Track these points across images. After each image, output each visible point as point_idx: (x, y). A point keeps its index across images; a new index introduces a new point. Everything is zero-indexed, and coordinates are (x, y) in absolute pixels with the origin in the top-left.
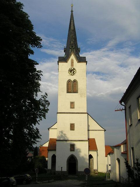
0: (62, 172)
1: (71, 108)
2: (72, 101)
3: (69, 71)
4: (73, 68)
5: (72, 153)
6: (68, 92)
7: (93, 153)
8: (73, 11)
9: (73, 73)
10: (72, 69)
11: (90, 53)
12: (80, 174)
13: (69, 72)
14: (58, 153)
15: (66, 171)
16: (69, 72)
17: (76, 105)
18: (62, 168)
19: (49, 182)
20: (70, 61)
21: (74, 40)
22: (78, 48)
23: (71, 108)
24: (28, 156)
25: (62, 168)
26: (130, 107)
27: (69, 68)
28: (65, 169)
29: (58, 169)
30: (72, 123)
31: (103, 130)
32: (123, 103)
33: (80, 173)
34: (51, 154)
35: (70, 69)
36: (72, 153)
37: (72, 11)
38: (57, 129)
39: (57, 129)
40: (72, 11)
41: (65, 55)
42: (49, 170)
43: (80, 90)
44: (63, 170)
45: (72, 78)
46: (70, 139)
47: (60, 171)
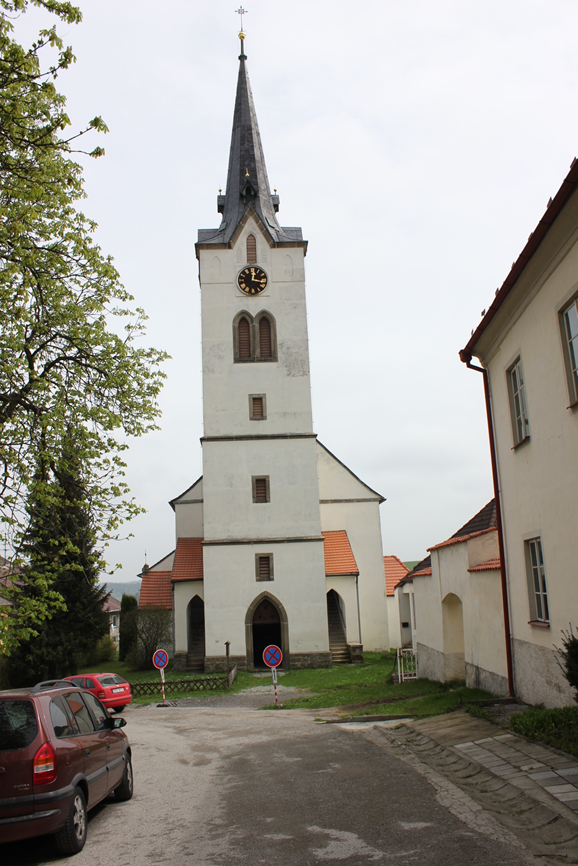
3: (240, 277)
5: (266, 587)
6: (237, 361)
7: (344, 589)
8: (246, 58)
9: (250, 273)
11: (277, 737)
14: (212, 594)
15: (244, 653)
17: (270, 407)
18: (227, 644)
20: (241, 242)
25: (227, 644)
26: (511, 373)
28: (240, 648)
29: (213, 648)
30: (261, 473)
31: (374, 500)
32: (475, 361)
33: (299, 660)
34: (182, 599)
36: (266, 587)
43: (284, 349)
44: (233, 652)
45: (254, 306)
46: (442, 563)
47: (222, 659)
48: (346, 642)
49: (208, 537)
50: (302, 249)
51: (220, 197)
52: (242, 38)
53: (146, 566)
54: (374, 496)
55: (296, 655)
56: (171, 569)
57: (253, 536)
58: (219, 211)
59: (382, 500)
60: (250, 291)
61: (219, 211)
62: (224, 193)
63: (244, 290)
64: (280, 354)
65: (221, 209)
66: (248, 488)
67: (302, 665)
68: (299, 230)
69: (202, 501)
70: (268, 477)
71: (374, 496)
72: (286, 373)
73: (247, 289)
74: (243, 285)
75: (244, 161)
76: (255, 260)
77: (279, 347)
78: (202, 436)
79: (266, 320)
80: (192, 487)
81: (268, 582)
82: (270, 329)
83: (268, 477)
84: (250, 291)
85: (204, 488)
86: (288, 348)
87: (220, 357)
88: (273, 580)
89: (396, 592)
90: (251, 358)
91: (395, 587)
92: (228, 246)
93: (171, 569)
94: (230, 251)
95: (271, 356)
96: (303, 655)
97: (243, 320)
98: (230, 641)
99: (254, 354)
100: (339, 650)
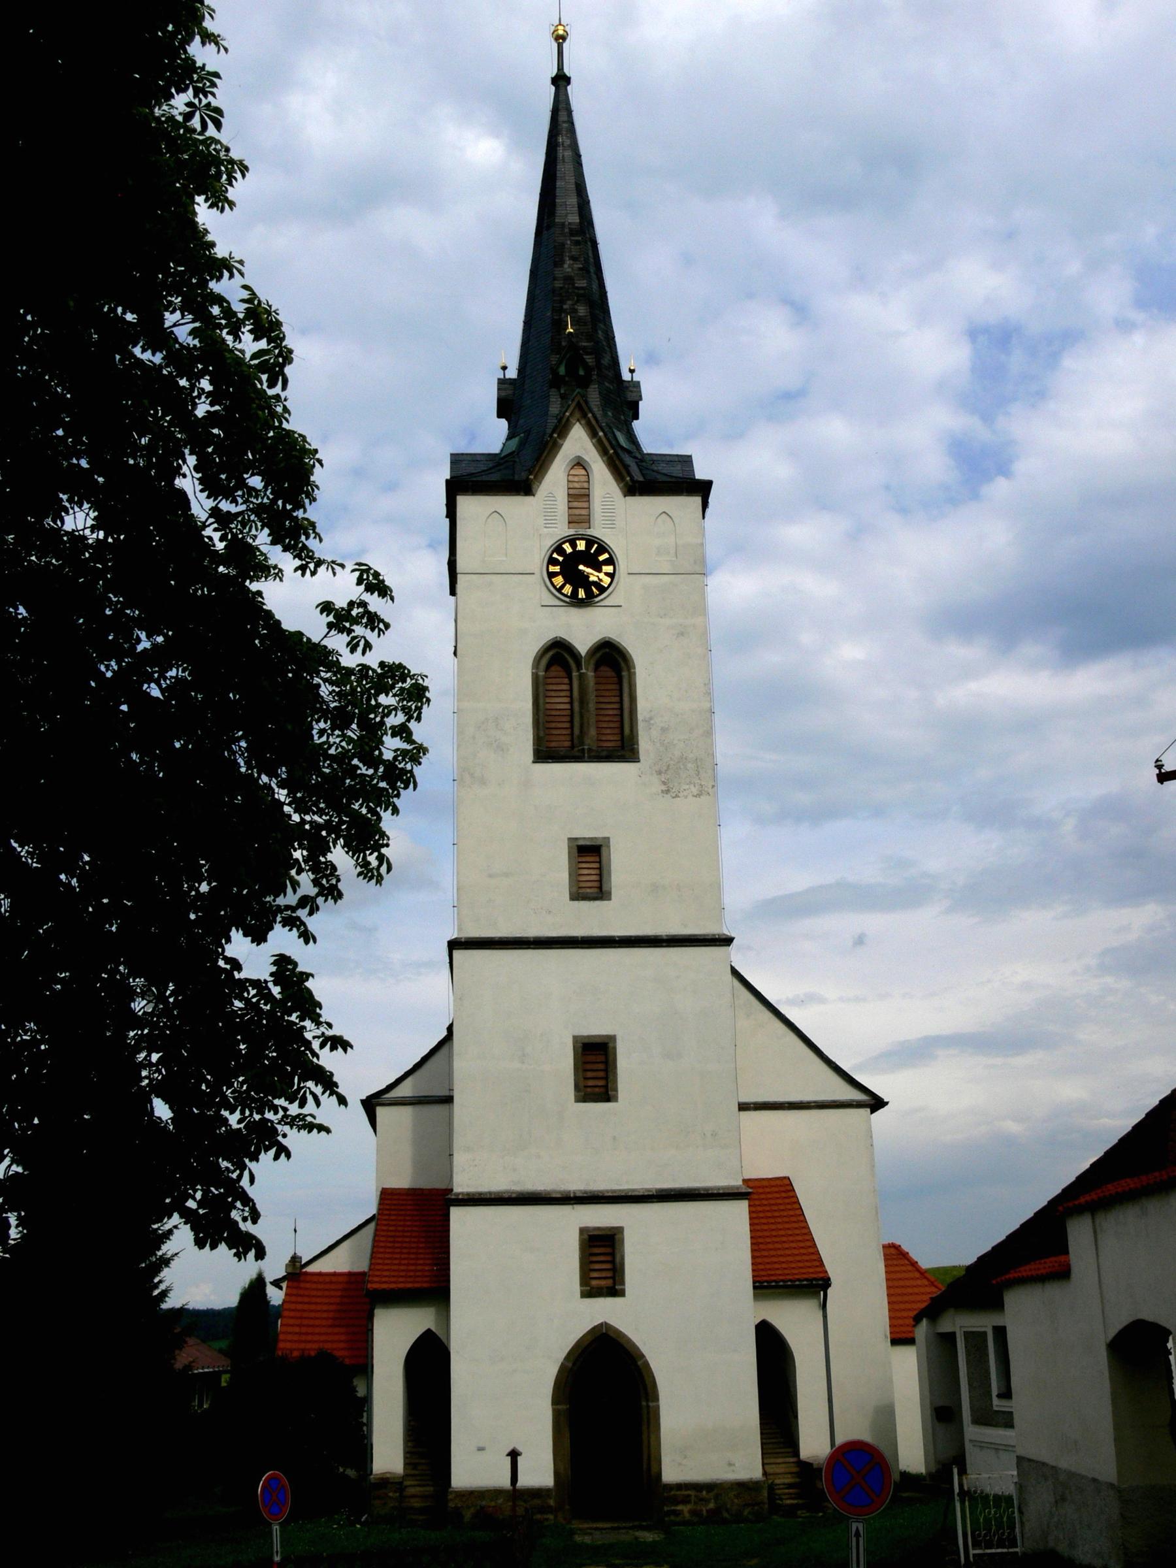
0: (516, 1494)
1: (578, 894)
2: (587, 832)
3: (552, 561)
4: (590, 542)
6: (545, 753)
8: (567, 80)
10: (581, 545)
12: (685, 1509)
13: (551, 575)
16: (551, 575)
18: (514, 1455)
19: (303, 1350)
21: (582, 310)
22: (626, 376)
23: (578, 894)
24: (247, 360)
25: (514, 1455)
27: (549, 542)
30: (596, 1029)
31: (858, 1105)
33: (686, 1500)
35: (559, 549)
36: (604, 1311)
37: (561, 80)
38: (743, 1107)
39: (743, 1107)
40: (561, 80)
41: (509, 438)
42: (385, 1482)
43: (655, 733)
44: (527, 1480)
47: (497, 1493)
48: (796, 1453)
49: (462, 1184)
50: (698, 500)
51: (502, 382)
52: (560, 39)
53: (295, 1259)
54: (851, 1094)
55: (680, 1486)
56: (366, 1269)
57: (575, 1184)
58: (499, 416)
59: (876, 1103)
60: (575, 593)
61: (499, 416)
62: (512, 373)
63: (560, 590)
64: (645, 744)
65: (505, 408)
66: (565, 1063)
67: (693, 1513)
68: (687, 461)
69: (448, 1100)
70: (613, 1038)
71: (851, 1094)
72: (657, 787)
73: (568, 589)
74: (559, 581)
75: (562, 302)
76: (587, 521)
77: (641, 726)
78: (454, 935)
79: (590, 1291)
80: (425, 1059)
81: (609, 1301)
82: (620, 683)
83: (613, 1038)
84: (574, 546)
85: (458, 1064)
86: (664, 730)
87: (501, 748)
88: (622, 1293)
89: (922, 1331)
90: (576, 752)
91: (917, 1320)
92: (525, 488)
93: (366, 1269)
94: (528, 499)
95: (623, 747)
96: (697, 1487)
97: (614, 1288)
98: (520, 1449)
99: (582, 743)
100: (784, 1476)
